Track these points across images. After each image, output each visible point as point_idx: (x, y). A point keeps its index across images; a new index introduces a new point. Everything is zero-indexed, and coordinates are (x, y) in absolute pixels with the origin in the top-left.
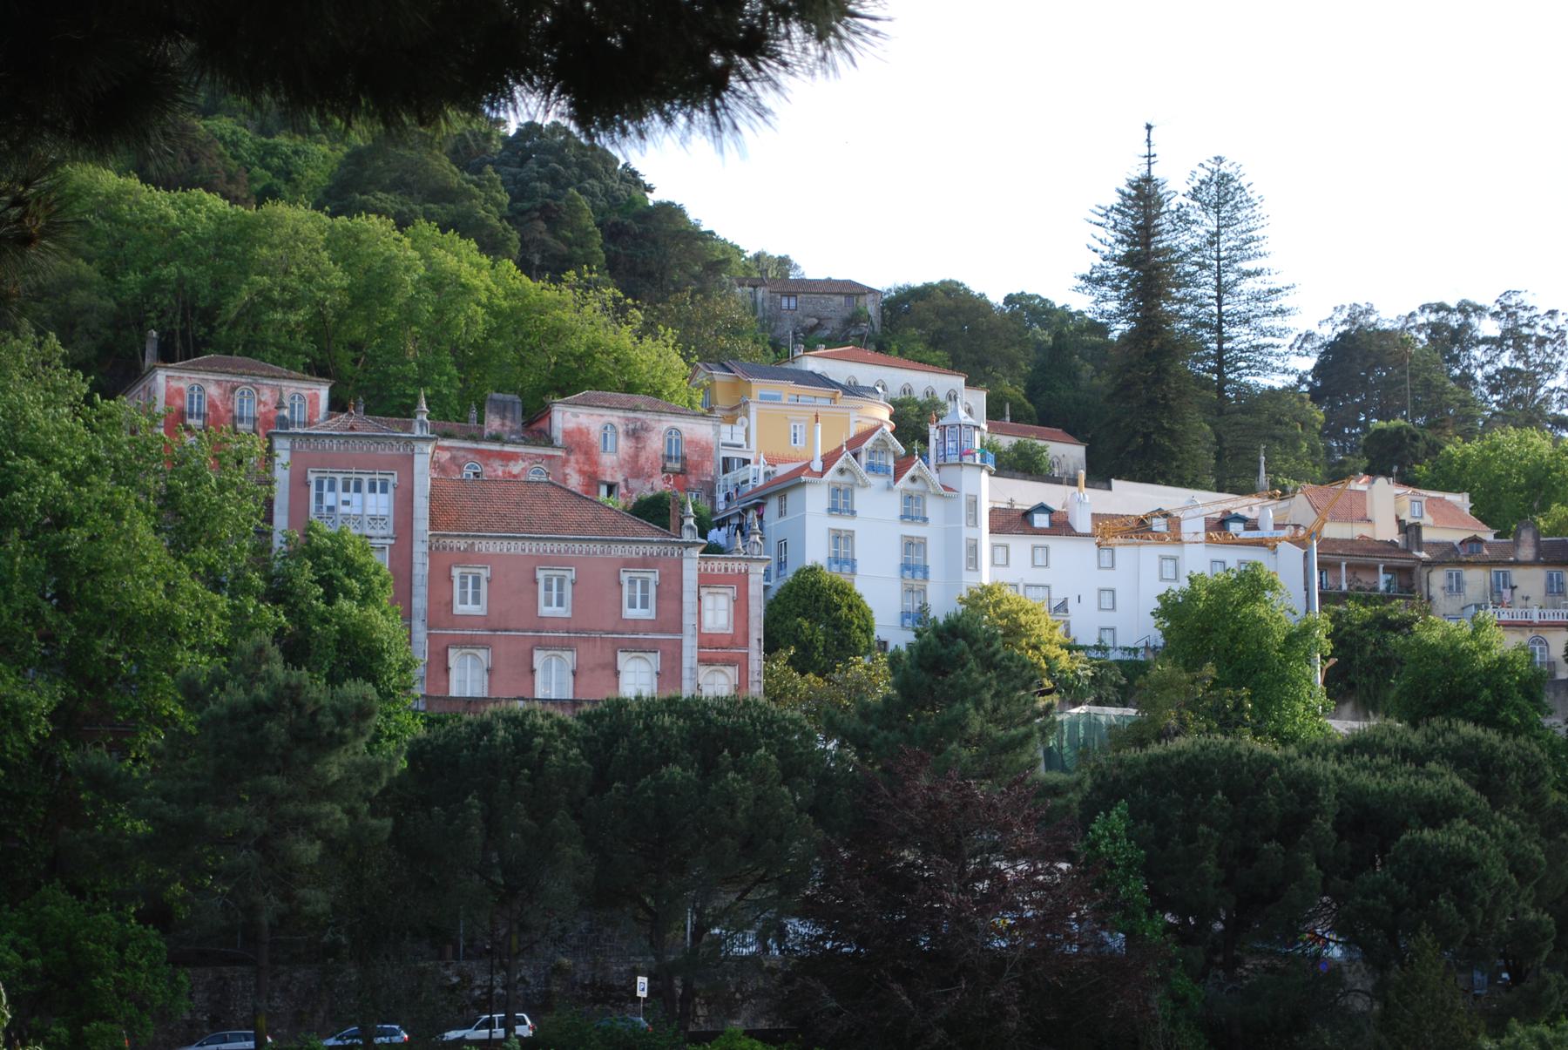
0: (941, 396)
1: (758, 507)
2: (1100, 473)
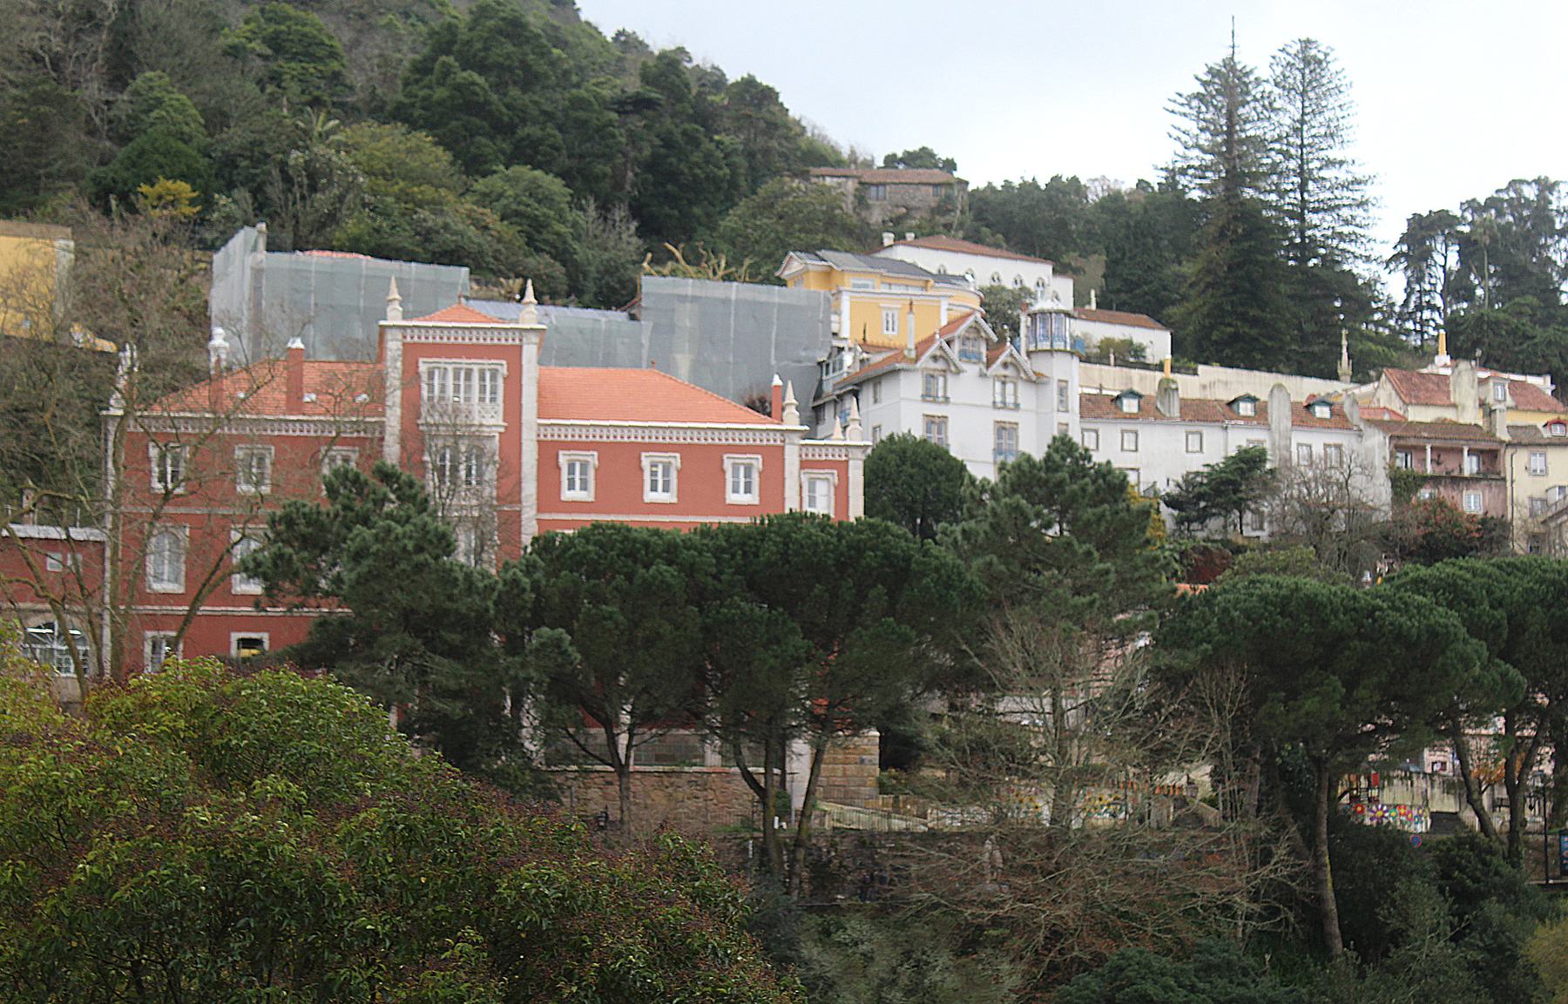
0: (1030, 284)
1: (856, 394)
2: (1189, 353)
